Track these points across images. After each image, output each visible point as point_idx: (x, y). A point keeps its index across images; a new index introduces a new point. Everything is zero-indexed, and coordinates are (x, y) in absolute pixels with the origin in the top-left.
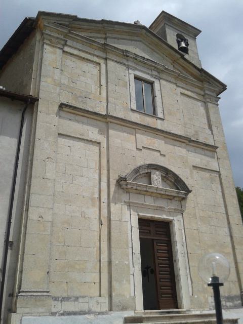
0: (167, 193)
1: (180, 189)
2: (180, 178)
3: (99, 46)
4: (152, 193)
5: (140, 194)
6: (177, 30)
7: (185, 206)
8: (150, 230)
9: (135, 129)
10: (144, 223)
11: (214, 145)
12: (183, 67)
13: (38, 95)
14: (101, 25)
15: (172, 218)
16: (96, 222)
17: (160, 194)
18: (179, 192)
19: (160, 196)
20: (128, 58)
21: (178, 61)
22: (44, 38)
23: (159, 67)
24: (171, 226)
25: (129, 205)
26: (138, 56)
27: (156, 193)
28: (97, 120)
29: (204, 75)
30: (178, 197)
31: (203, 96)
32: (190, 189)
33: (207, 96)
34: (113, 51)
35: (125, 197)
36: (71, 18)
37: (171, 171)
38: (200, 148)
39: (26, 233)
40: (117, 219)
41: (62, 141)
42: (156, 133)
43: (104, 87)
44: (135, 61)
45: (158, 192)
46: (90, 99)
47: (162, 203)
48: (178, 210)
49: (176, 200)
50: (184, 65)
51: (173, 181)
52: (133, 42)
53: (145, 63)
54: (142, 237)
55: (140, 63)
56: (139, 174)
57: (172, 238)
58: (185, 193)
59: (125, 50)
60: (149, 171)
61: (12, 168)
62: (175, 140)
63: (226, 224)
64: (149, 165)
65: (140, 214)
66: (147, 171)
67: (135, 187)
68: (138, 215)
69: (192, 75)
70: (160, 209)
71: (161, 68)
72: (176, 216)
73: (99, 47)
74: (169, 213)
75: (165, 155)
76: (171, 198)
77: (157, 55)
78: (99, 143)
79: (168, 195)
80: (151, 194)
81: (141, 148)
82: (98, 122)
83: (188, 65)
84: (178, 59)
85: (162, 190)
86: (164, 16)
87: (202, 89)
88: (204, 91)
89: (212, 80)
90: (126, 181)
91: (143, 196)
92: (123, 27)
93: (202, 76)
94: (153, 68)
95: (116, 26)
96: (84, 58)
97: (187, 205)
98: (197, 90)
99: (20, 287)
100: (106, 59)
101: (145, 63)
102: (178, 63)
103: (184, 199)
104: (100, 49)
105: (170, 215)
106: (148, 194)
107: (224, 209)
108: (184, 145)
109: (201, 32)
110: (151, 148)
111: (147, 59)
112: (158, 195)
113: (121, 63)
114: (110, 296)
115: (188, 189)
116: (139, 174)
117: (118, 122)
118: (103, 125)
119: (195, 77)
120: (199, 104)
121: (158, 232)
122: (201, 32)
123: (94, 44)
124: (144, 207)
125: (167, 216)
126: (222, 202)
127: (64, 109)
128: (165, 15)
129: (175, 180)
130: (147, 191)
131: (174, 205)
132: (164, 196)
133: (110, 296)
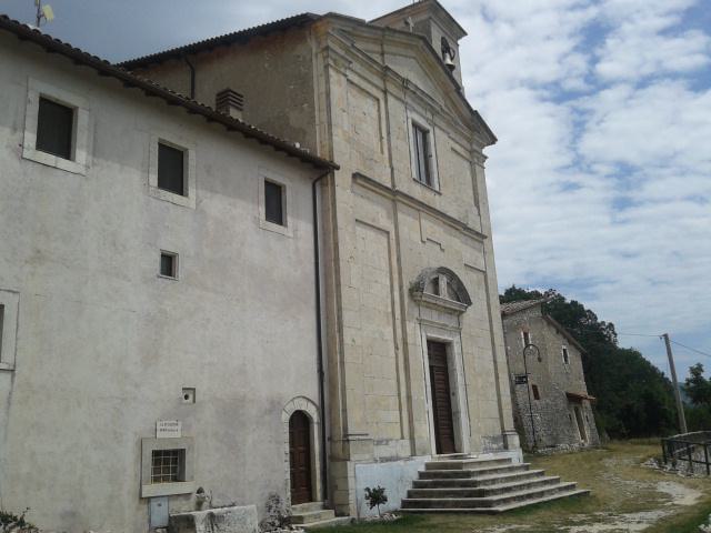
9: (419, 210)
10: (431, 343)
11: (389, 185)
13: (331, 156)
15: (450, 339)
16: (392, 345)
22: (328, 56)
24: (448, 350)
39: (405, 343)
41: (360, 229)
43: (385, 141)
53: (422, 100)
57: (449, 365)
61: (312, 267)
63: (490, 346)
69: (461, 116)
71: (438, 109)
77: (430, 84)
78: (388, 233)
83: (460, 101)
87: (470, 141)
88: (471, 144)
93: (472, 121)
98: (464, 142)
99: (345, 429)
100: (385, 92)
103: (462, 312)
104: (377, 73)
107: (488, 324)
109: (465, 34)
114: (412, 439)
118: (389, 204)
119: (464, 121)
122: (465, 34)
124: (431, 324)
126: (487, 315)
127: (359, 181)
129: (458, 289)
133: (412, 439)
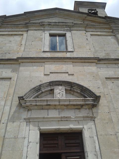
0: (71, 103)
1: (87, 96)
2: (85, 87)
3: (23, 26)
4: (55, 105)
5: (42, 109)
6: (88, 7)
7: (97, 112)
8: (57, 144)
12: (91, 21)
14: (25, 16)
15: (81, 127)
17: (65, 105)
18: (85, 100)
19: (65, 107)
20: (44, 26)
21: (87, 19)
23: (68, 24)
25: (28, 121)
26: (51, 22)
27: (59, 105)
28: (12, 64)
29: (109, 20)
30: (87, 105)
31: (112, 32)
32: (98, 95)
33: (114, 31)
34: (33, 25)
35: (25, 115)
36: (3, 18)
37: (74, 83)
38: (113, 63)
40: (12, 136)
42: (65, 61)
44: (50, 26)
45: (61, 103)
46: (9, 53)
47: (71, 114)
48: (88, 117)
49: (86, 109)
50: (91, 19)
51: (79, 91)
52: (50, 19)
53: (58, 25)
54: (42, 152)
55: (54, 27)
56: (41, 92)
58: (92, 100)
59: (41, 22)
60: (52, 88)
62: (85, 62)
64: (50, 82)
65: (41, 128)
66: (50, 88)
67: (34, 104)
68: (40, 129)
70: (67, 119)
71: (71, 24)
72: (87, 124)
73: (23, 27)
74: (78, 121)
75: (73, 74)
76: (79, 107)
79: (74, 105)
80: (55, 107)
81: (49, 73)
82: (13, 65)
84: (86, 18)
85: (65, 101)
86: (77, 4)
87: (110, 28)
89: (116, 20)
90: (23, 99)
91: (47, 110)
92: (41, 13)
94: (65, 26)
95: (36, 14)
96: (12, 35)
97: (99, 111)
101: (58, 25)
102: (87, 20)
104: (23, 27)
105: (78, 122)
106: (52, 107)
108: (94, 64)
109: (106, 3)
110: (58, 71)
111: (57, 22)
112: (63, 106)
113: (38, 30)
115: (95, 95)
116: (41, 92)
117: (29, 61)
120: (110, 37)
121: (68, 145)
123: (19, 26)
125: (74, 125)
128: (77, 3)
129: (82, 91)
130: (49, 105)
131: (84, 113)
132: (69, 107)
